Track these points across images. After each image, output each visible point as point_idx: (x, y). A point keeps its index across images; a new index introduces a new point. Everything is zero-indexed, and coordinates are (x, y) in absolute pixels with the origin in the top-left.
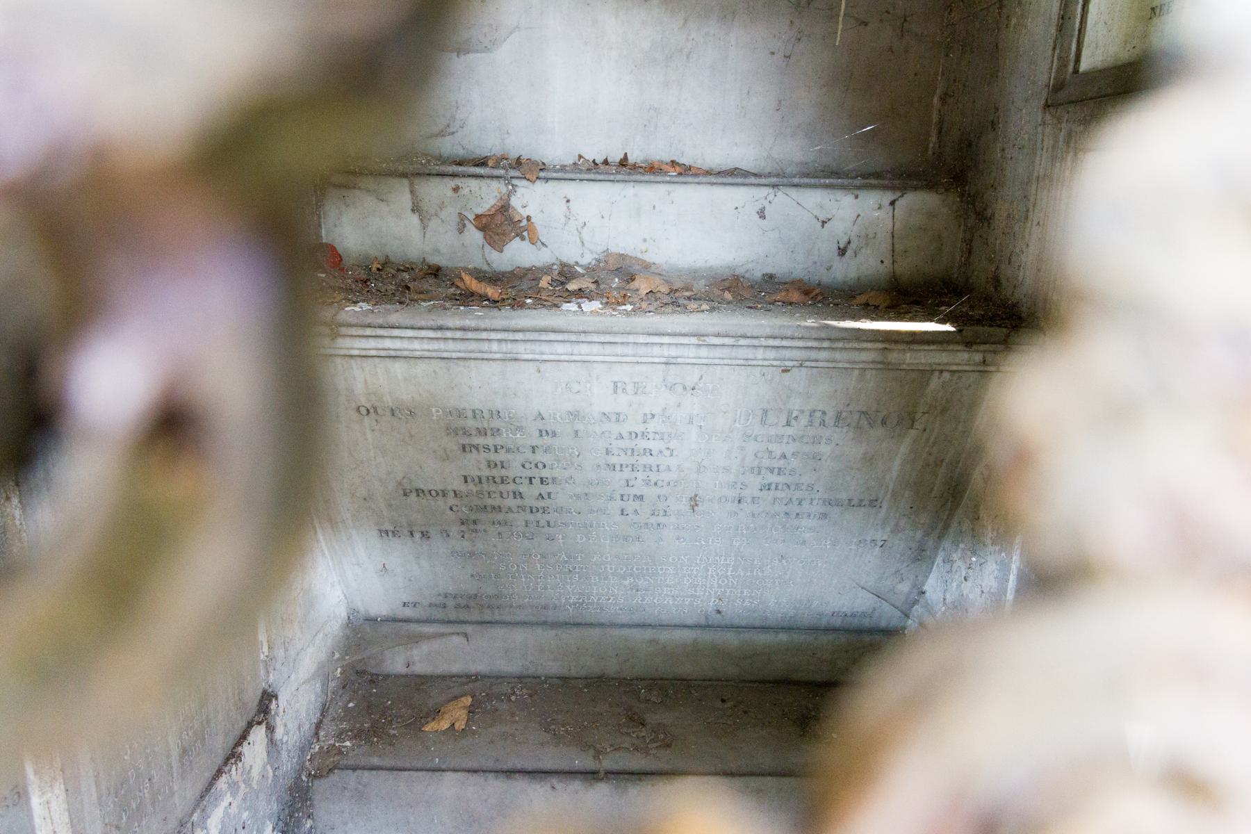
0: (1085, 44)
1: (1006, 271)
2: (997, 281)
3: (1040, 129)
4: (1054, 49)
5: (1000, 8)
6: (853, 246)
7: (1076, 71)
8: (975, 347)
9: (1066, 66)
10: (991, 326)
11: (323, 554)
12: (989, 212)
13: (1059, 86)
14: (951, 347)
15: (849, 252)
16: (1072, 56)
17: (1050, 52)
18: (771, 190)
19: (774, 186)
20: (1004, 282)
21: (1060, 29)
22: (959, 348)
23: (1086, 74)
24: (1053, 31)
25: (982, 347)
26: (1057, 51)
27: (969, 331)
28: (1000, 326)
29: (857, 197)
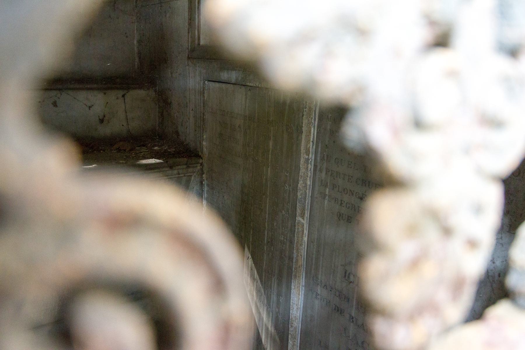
0: (201, 32)
1: (181, 129)
2: (177, 133)
3: (187, 67)
4: (189, 33)
5: (161, 7)
6: (106, 118)
7: (199, 44)
8: (174, 168)
9: (194, 41)
10: (179, 157)
11: (271, 334)
12: (169, 101)
13: (193, 50)
14: (164, 169)
15: (105, 122)
16: (197, 37)
17: (187, 34)
18: (58, 92)
19: (60, 90)
20: (180, 133)
21: (190, 24)
22: (167, 169)
23: (203, 46)
24: (187, 24)
25: (177, 167)
26: (190, 34)
27: (171, 161)
28: (183, 157)
29: (105, 94)
